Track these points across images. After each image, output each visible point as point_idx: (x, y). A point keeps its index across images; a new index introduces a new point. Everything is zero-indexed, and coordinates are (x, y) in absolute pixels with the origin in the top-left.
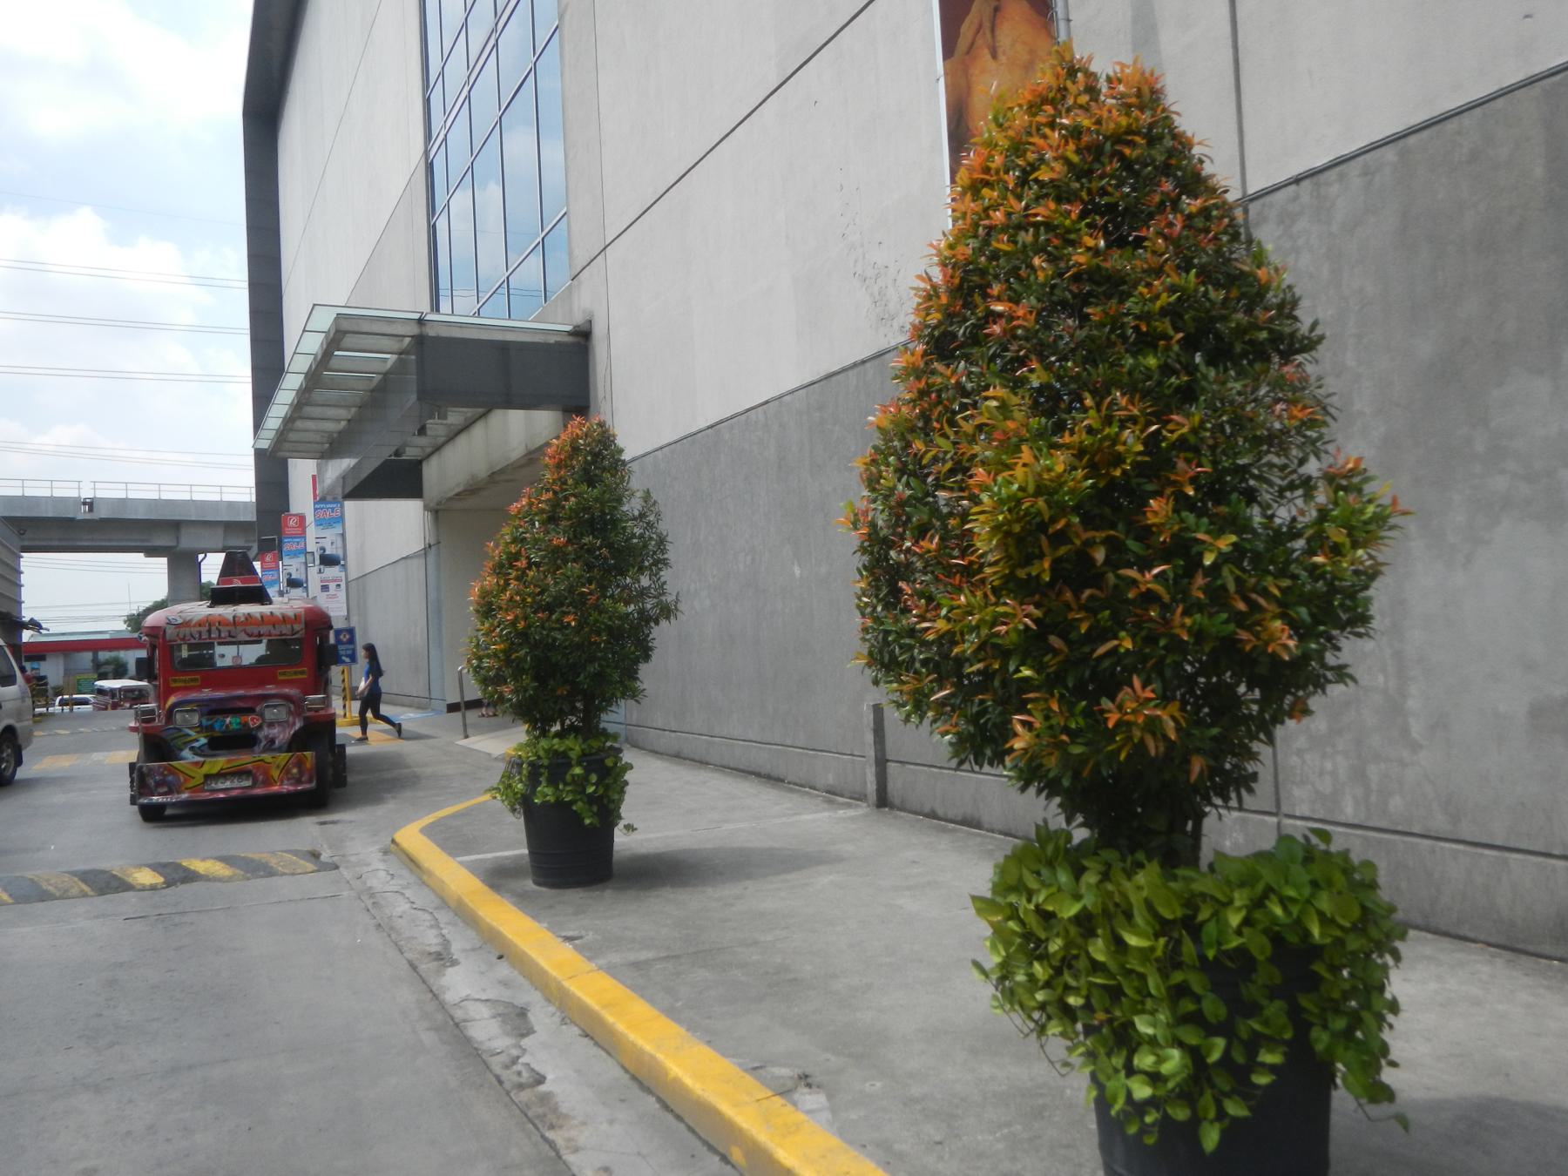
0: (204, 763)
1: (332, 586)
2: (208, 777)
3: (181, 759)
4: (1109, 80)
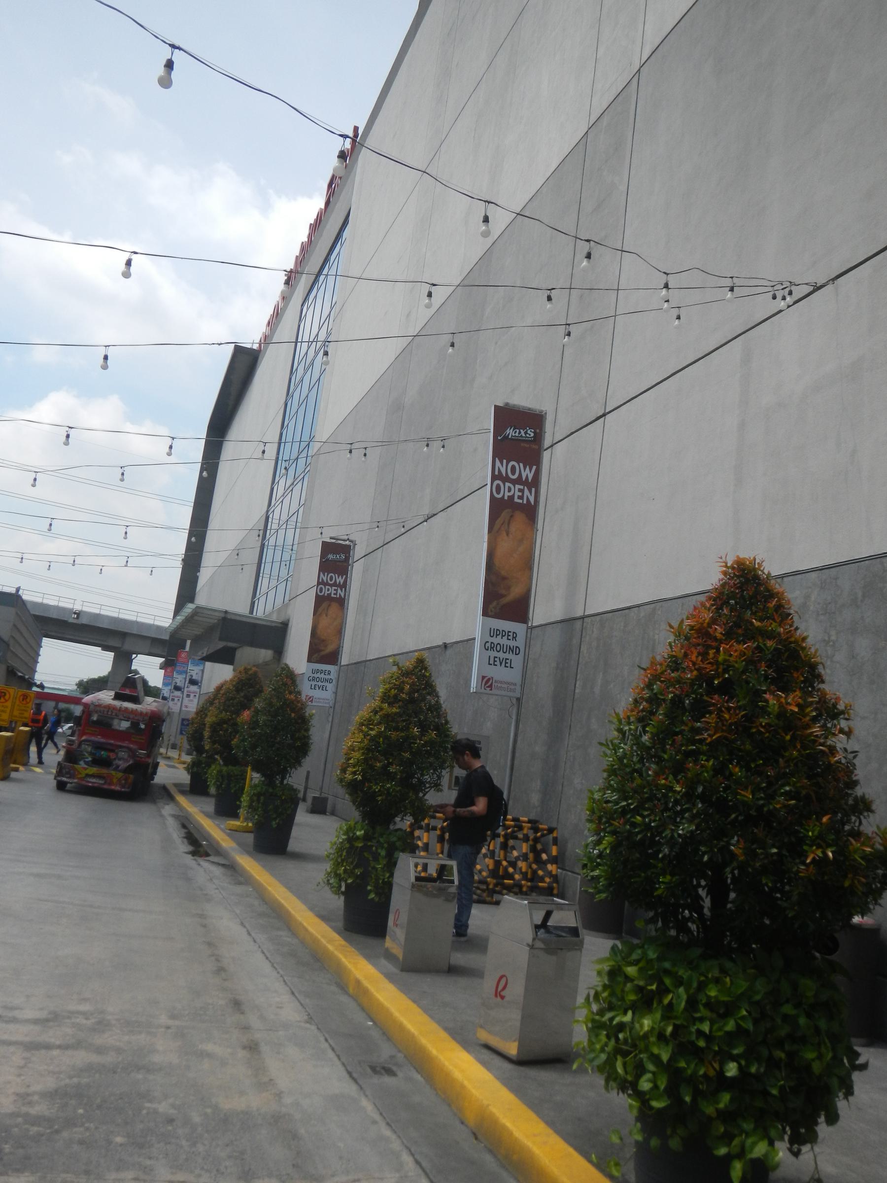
0: (87, 768)
1: (192, 695)
2: (87, 775)
3: (79, 764)
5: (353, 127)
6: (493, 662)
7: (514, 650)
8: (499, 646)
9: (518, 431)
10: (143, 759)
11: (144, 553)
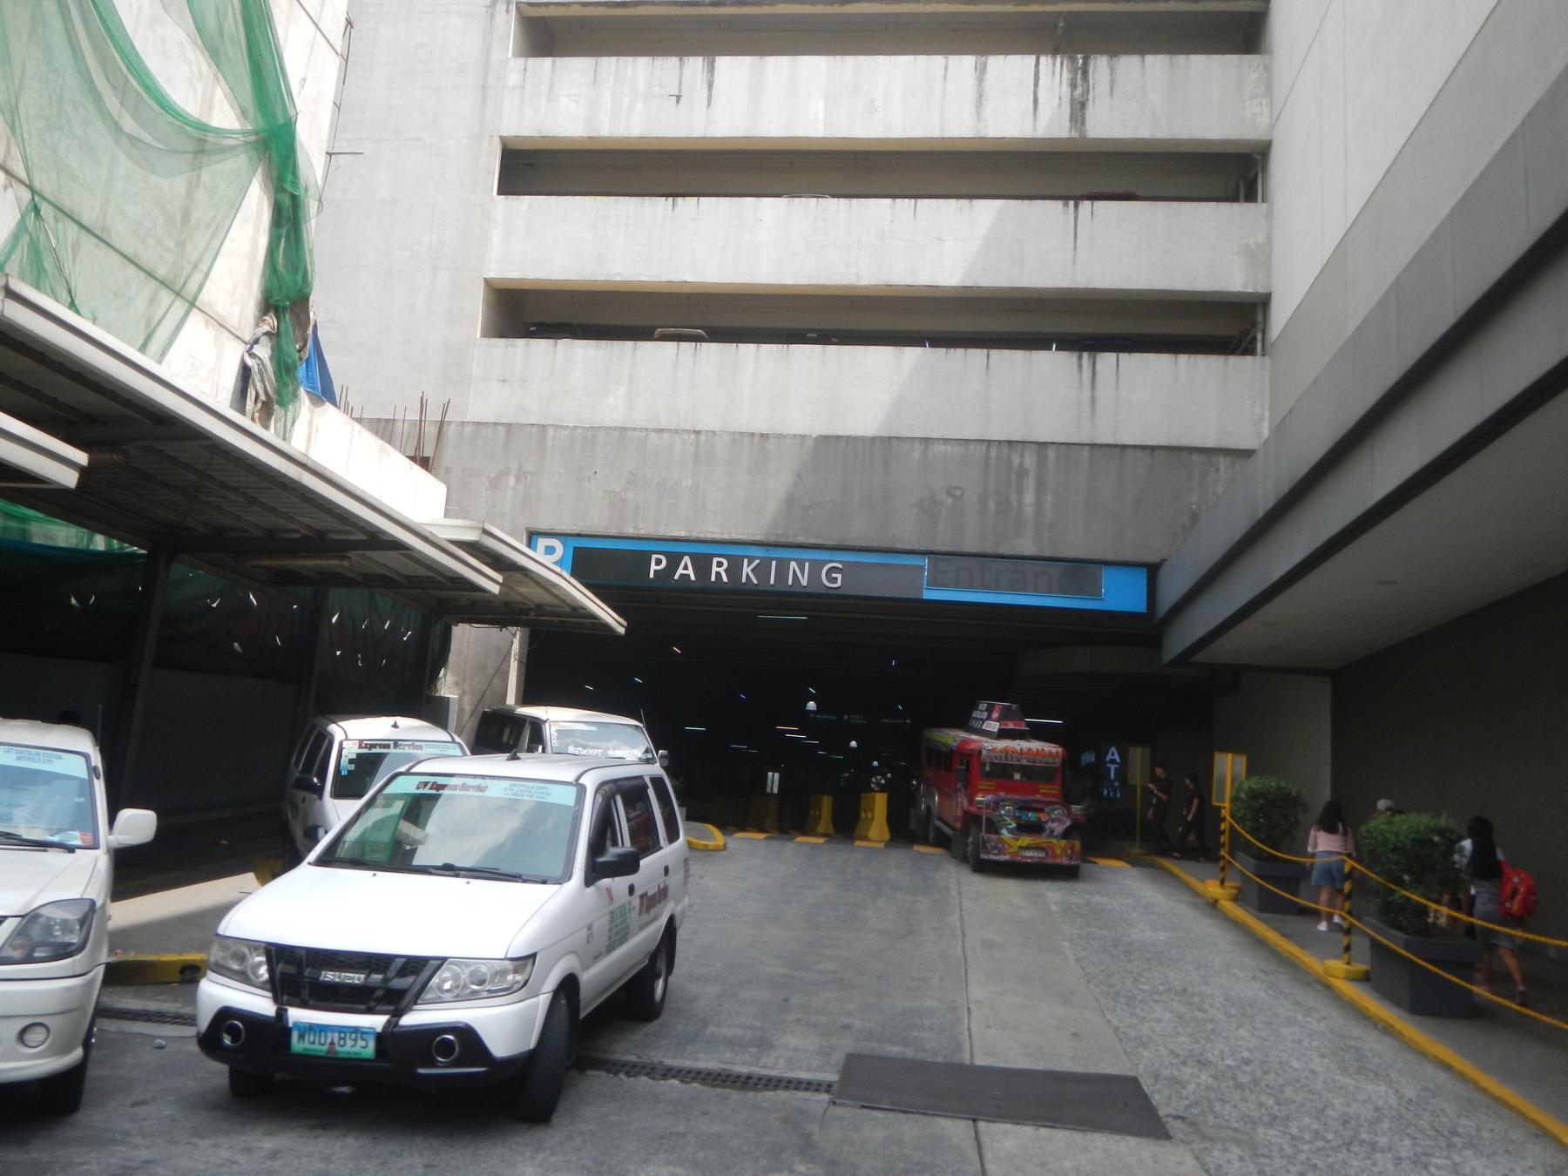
2: (1021, 848)
4: (359, 748)
5: (481, 286)
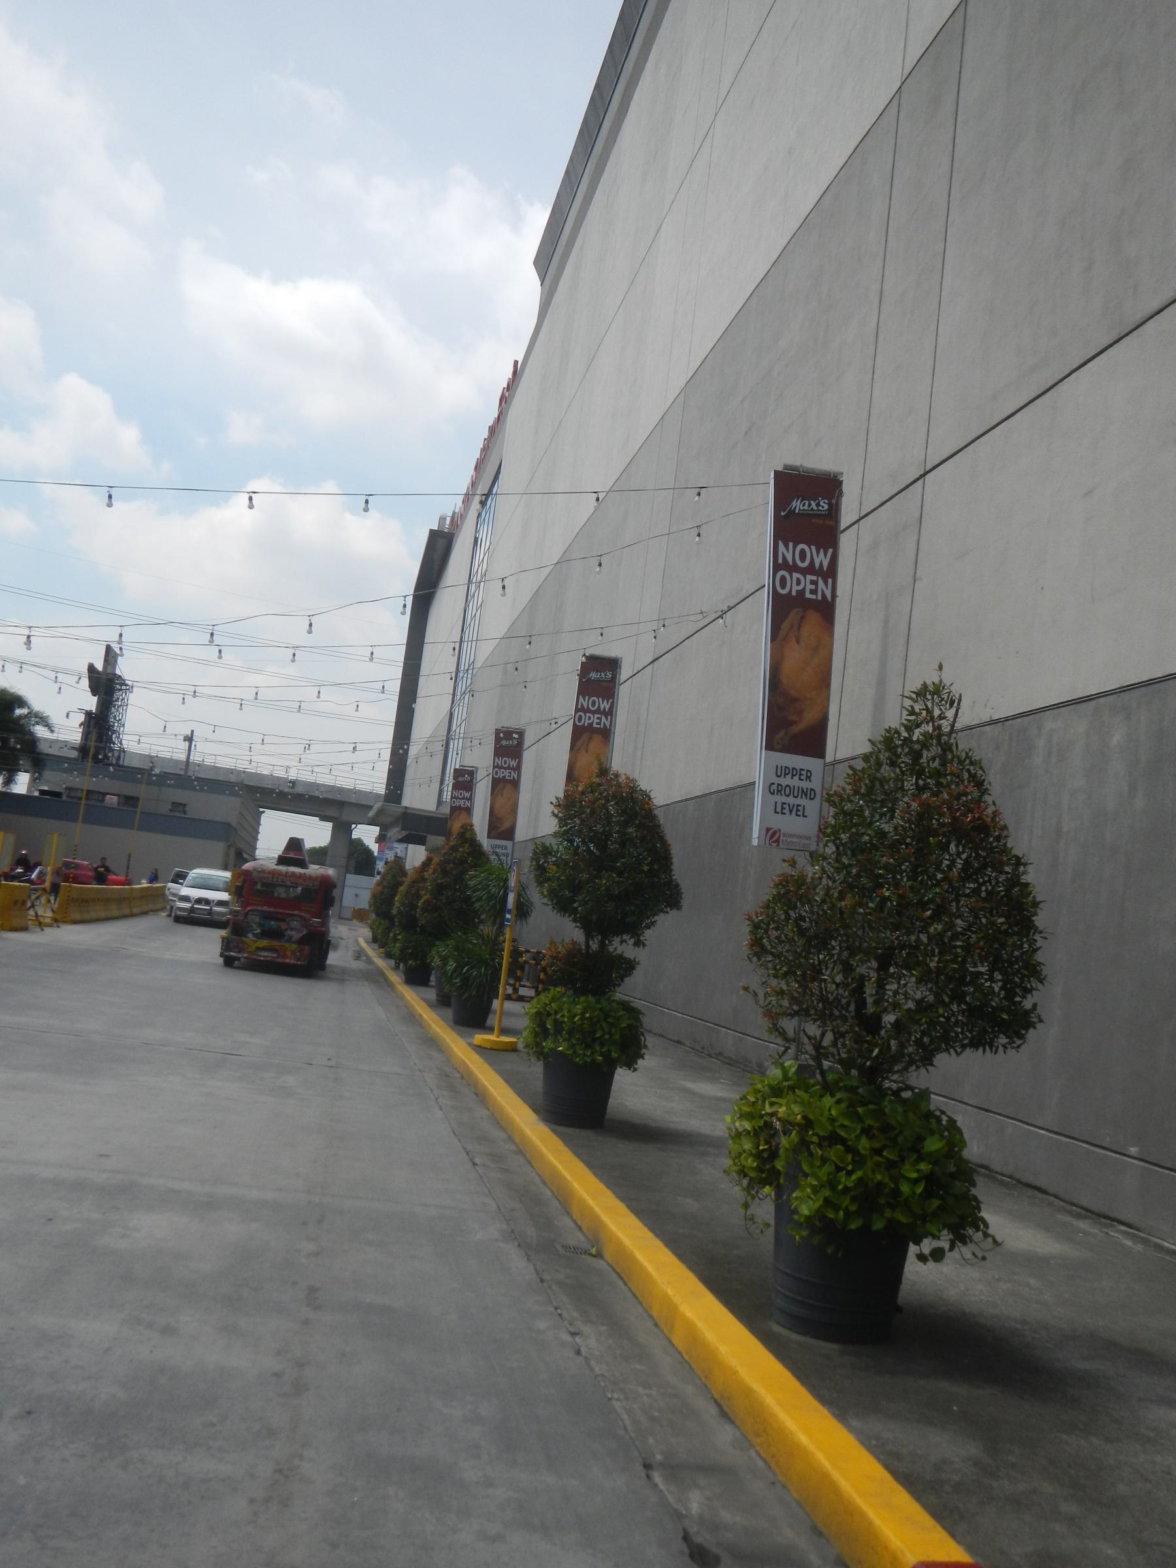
2: (258, 949)
6: (780, 810)
7: (808, 794)
8: (788, 789)
9: (807, 502)
10: (318, 928)
11: (319, 651)
